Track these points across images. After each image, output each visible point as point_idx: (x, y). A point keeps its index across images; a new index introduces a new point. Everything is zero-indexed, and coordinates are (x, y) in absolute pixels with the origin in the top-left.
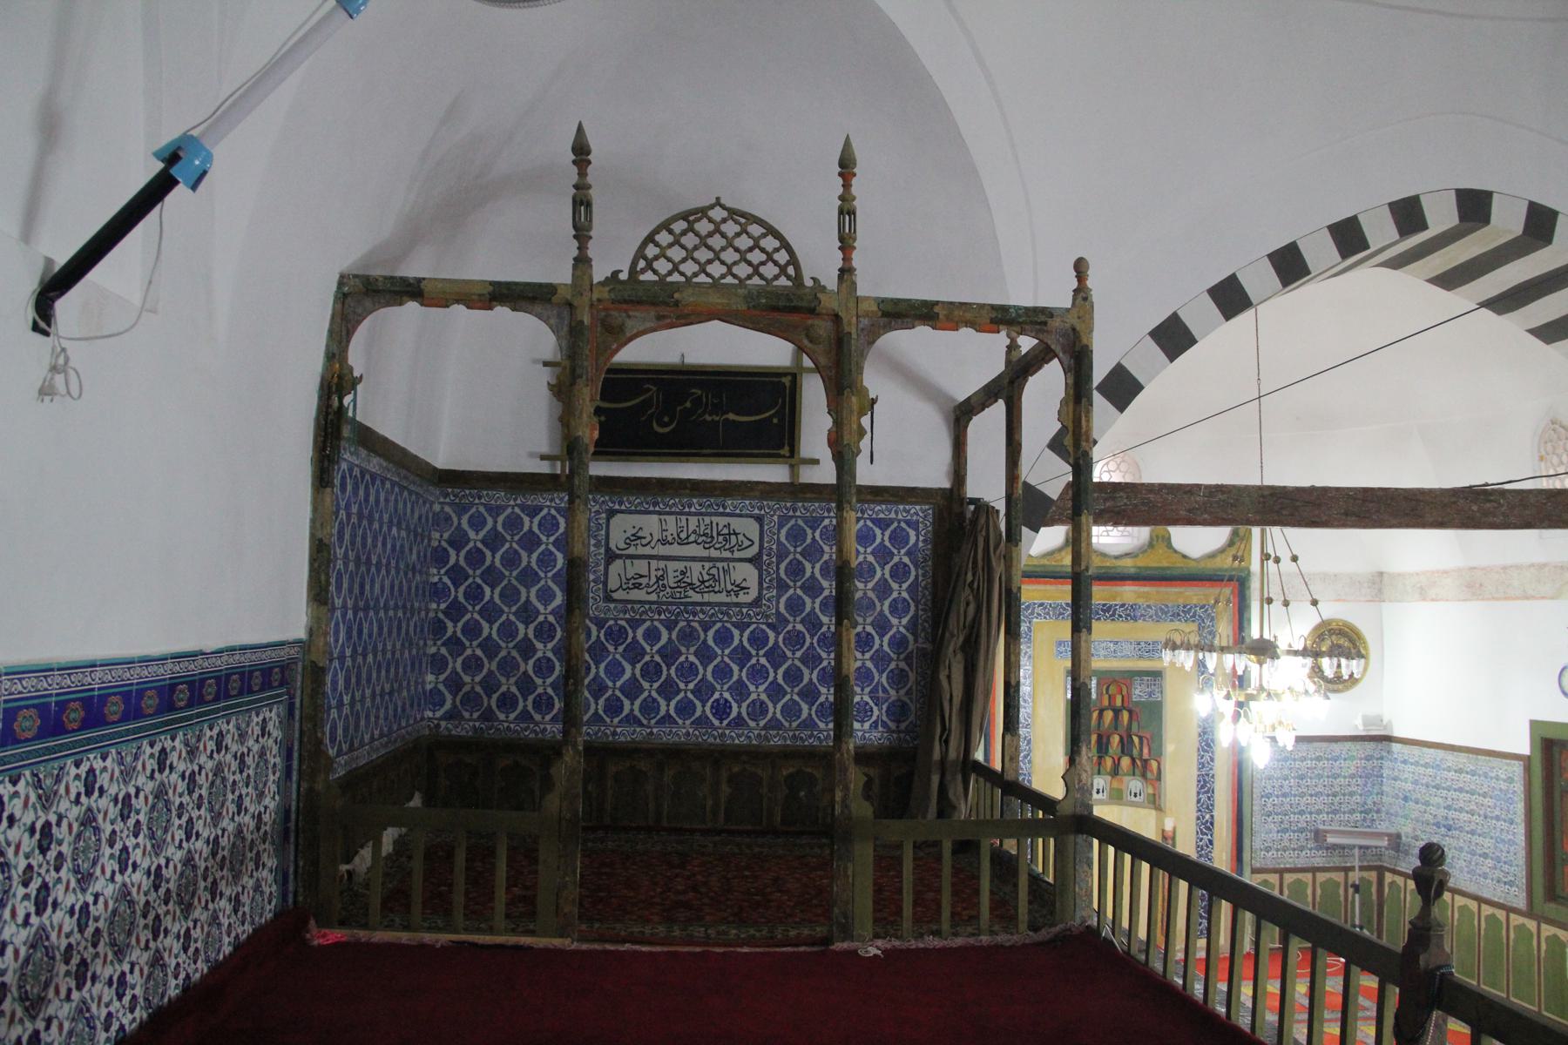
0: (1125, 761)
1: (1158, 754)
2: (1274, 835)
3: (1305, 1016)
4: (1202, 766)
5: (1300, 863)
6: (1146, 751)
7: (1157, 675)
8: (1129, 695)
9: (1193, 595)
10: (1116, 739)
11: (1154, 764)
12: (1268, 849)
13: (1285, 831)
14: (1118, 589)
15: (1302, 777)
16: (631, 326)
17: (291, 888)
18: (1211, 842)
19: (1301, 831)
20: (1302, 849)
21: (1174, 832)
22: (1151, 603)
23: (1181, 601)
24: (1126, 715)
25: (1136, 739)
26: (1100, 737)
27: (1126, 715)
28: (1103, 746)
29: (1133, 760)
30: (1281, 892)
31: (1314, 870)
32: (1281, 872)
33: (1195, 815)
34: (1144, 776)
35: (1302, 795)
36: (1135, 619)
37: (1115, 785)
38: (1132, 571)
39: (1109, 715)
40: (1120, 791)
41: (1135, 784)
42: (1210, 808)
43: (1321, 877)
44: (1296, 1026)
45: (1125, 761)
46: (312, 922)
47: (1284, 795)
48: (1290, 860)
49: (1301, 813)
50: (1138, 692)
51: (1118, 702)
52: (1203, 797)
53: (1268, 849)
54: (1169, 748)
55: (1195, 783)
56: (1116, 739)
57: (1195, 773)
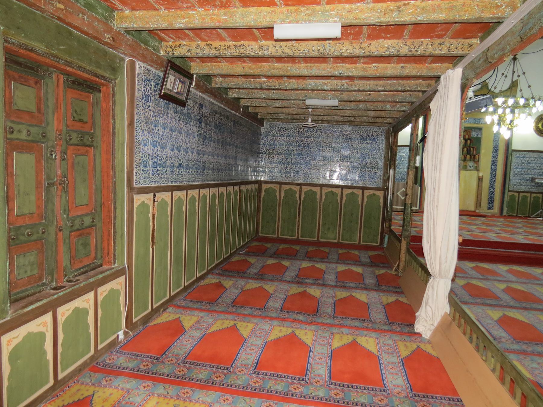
0: (468, 157)
1: (478, 153)
2: (518, 181)
4: (448, 24)
5: (526, 190)
6: (475, 152)
7: (480, 129)
8: (470, 135)
12: (515, 185)
13: (521, 180)
15: (529, 163)
17: (392, 289)
18: (495, 181)
19: (528, 180)
20: (527, 186)
21: (483, 176)
24: (469, 141)
25: (472, 149)
27: (469, 141)
29: (471, 156)
30: (132, 64)
31: (531, 193)
32: (519, 192)
33: (490, 172)
34: (474, 161)
35: (529, 169)
37: (465, 164)
41: (471, 164)
42: (495, 170)
43: (534, 195)
45: (468, 157)
46: (391, 299)
47: (522, 169)
48: (523, 189)
49: (528, 174)
50: (474, 134)
52: (493, 167)
53: (515, 185)
54: (483, 151)
57: (491, 159)
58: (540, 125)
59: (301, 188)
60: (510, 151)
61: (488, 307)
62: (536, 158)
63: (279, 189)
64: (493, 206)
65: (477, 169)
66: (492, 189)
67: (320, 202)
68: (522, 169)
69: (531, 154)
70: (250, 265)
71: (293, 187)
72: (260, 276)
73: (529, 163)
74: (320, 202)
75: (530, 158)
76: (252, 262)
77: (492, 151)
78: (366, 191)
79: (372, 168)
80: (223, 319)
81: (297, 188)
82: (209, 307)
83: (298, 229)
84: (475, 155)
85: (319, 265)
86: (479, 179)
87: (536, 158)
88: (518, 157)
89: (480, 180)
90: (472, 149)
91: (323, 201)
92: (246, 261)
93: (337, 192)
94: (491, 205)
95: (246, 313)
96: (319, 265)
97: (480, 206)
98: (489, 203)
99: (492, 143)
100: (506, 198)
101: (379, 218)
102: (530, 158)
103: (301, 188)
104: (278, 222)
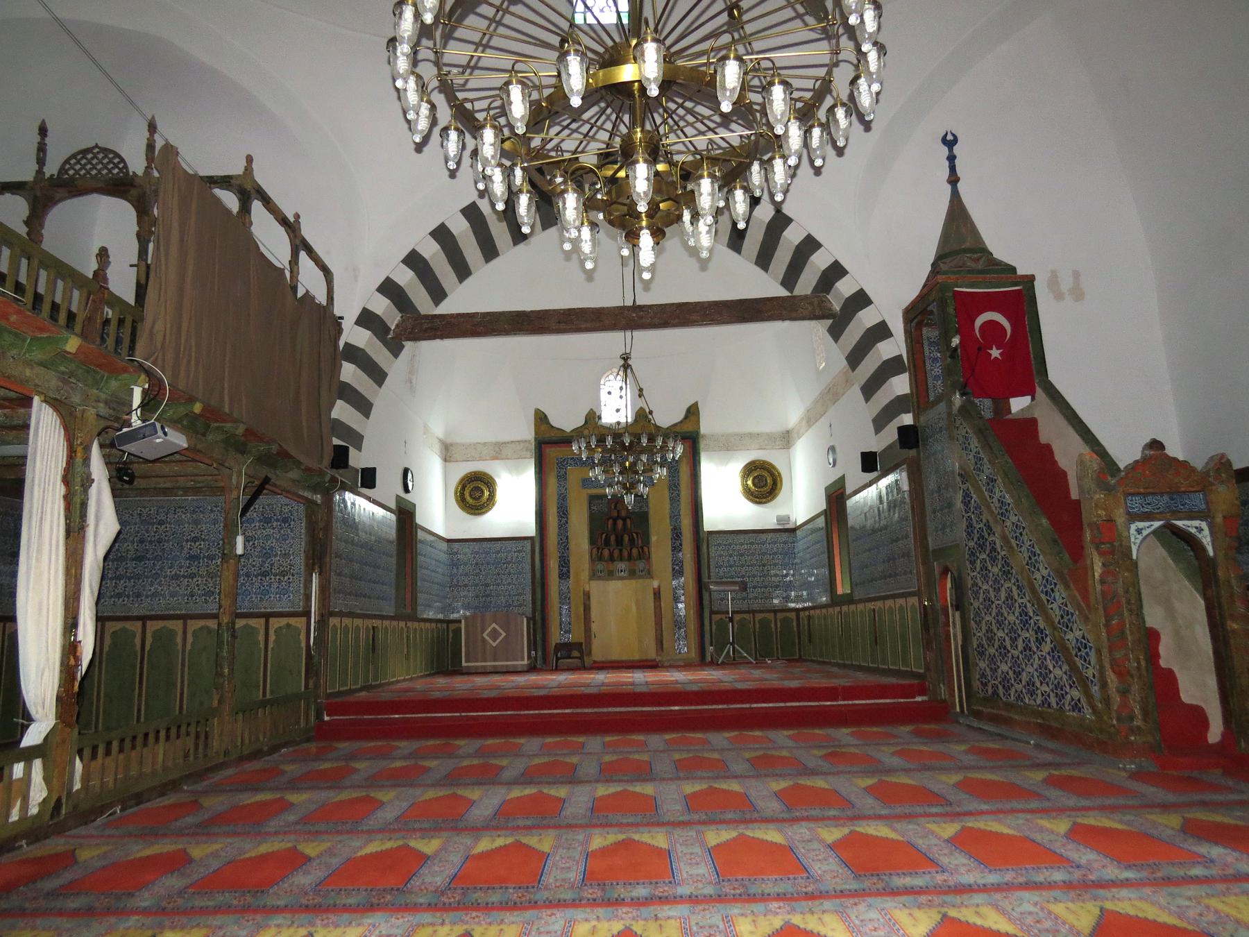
0: (635, 551)
10: (626, 538)
15: (742, 555)
24: (628, 522)
28: (619, 542)
35: (743, 566)
39: (620, 523)
56: (626, 538)
58: (750, 483)
59: (144, 626)
61: (820, 824)
62: (752, 543)
63: (140, 630)
67: (184, 651)
68: (731, 566)
69: (742, 536)
70: (379, 804)
71: (129, 625)
72: (403, 825)
73: (742, 555)
74: (184, 651)
75: (742, 544)
76: (475, 798)
78: (272, 620)
79: (283, 574)
80: (433, 924)
81: (136, 627)
82: (249, 899)
83: (139, 710)
85: (553, 791)
87: (752, 543)
88: (719, 545)
91: (188, 647)
92: (367, 799)
93: (133, 628)
95: (351, 901)
96: (553, 791)
97: (662, 648)
99: (668, 521)
101: (300, 673)
102: (742, 544)
103: (144, 626)
104: (98, 700)
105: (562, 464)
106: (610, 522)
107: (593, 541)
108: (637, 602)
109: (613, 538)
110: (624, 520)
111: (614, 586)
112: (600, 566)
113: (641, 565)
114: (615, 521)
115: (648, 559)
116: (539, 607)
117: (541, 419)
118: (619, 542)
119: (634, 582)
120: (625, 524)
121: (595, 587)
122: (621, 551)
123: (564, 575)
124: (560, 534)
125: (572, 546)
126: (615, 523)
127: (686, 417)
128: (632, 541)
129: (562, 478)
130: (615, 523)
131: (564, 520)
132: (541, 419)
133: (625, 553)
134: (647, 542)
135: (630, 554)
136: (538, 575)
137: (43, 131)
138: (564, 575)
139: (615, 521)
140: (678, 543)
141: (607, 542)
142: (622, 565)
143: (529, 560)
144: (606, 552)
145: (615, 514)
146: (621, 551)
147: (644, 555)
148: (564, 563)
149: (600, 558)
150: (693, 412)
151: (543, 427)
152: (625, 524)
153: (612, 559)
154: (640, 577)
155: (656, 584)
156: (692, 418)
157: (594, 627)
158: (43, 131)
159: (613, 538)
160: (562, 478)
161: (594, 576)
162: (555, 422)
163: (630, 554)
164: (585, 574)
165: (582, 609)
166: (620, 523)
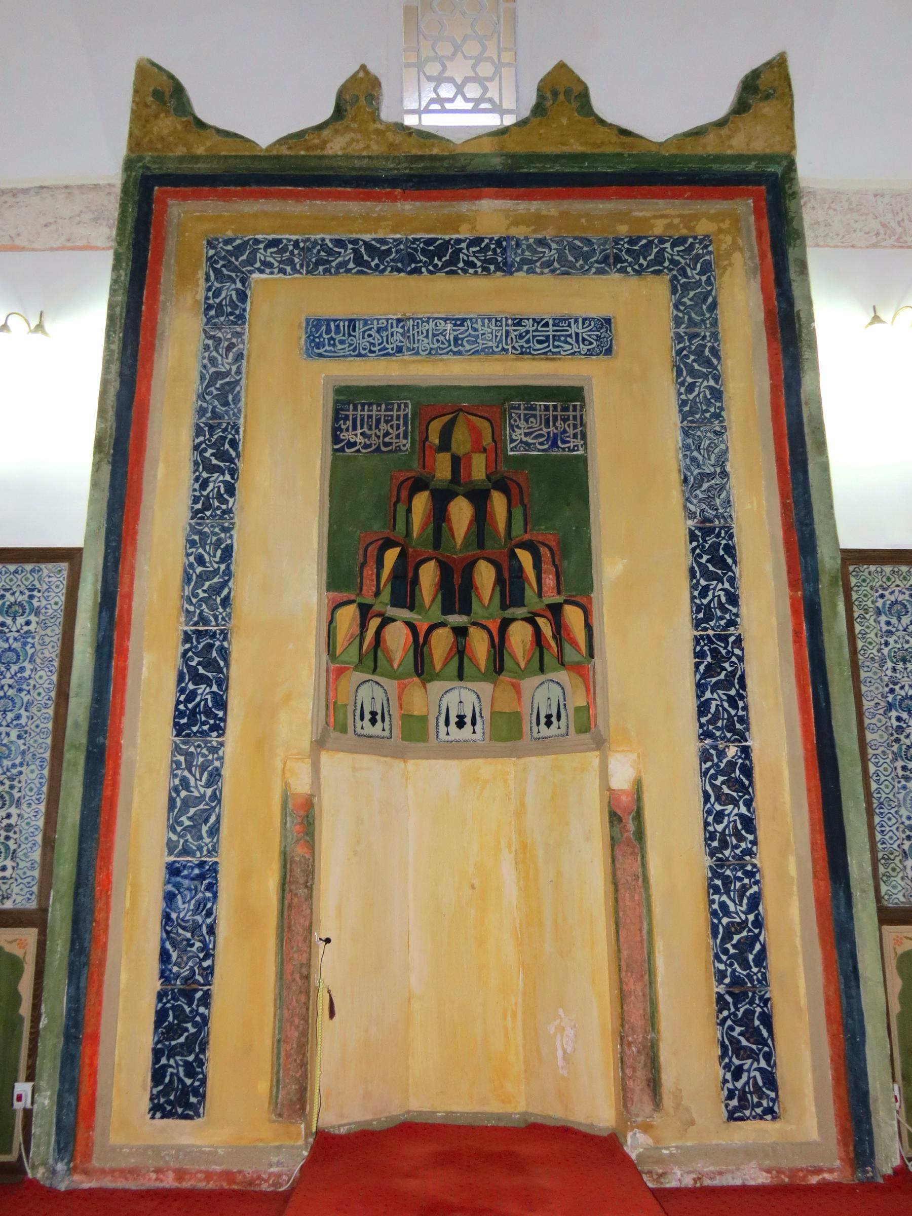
0: (520, 636)
3: (869, 737)
4: (703, 615)
7: (570, 398)
9: (658, 215)
10: (485, 576)
11: (573, 616)
14: (464, 207)
16: (97, 455)
18: (749, 823)
21: (638, 785)
22: (548, 233)
23: (623, 230)
24: (498, 503)
25: (525, 558)
26: (445, 569)
28: (457, 593)
36: (506, 268)
37: (506, 705)
38: (497, 163)
39: (461, 512)
40: (515, 718)
44: (424, 123)
51: (478, 470)
52: (717, 699)
55: (689, 661)
56: (485, 576)
57: (687, 632)
60: (827, 560)
64: (770, 1081)
65: (588, 727)
66: (738, 910)
77: (687, 560)
84: (556, 610)
86: (614, 818)
89: (625, 823)
90: (525, 558)
93: (18, 952)
94: (753, 1069)
97: (654, 1085)
98: (730, 1049)
100: (878, 993)
105: (231, 263)
106: (421, 503)
107: (341, 575)
108: (524, 855)
109: (428, 575)
110: (479, 499)
111: (431, 779)
112: (371, 693)
113: (542, 692)
114: (441, 500)
115: (583, 667)
116: (65, 870)
117: (160, 95)
118: (457, 593)
119: (510, 766)
120: (481, 516)
121: (349, 783)
122: (460, 632)
123: (200, 714)
124: (196, 539)
125: (245, 589)
126: (439, 514)
127: (741, 107)
128: (511, 588)
129: (226, 313)
130: (439, 514)
131: (217, 481)
132: (160, 95)
133: (479, 644)
134: (579, 587)
135: (499, 647)
136: (79, 708)
137: (329, 992)
138: (200, 714)
139: (441, 500)
140: (718, 590)
141: (404, 590)
142: (462, 697)
143: (52, 651)
144: (397, 638)
145: (442, 469)
146: (460, 632)
147: (563, 646)
148: (205, 664)
149: (373, 657)
150: (765, 89)
151: (166, 124)
152: (481, 516)
153: (421, 665)
154: (544, 746)
155: (621, 776)
156: (767, 109)
157: (331, 969)
158: (329, 992)
159: (428, 575)
160: (226, 313)
161: (339, 725)
162: (209, 106)
163: (499, 647)
164: (298, 719)
165: (272, 883)
166: (461, 512)
